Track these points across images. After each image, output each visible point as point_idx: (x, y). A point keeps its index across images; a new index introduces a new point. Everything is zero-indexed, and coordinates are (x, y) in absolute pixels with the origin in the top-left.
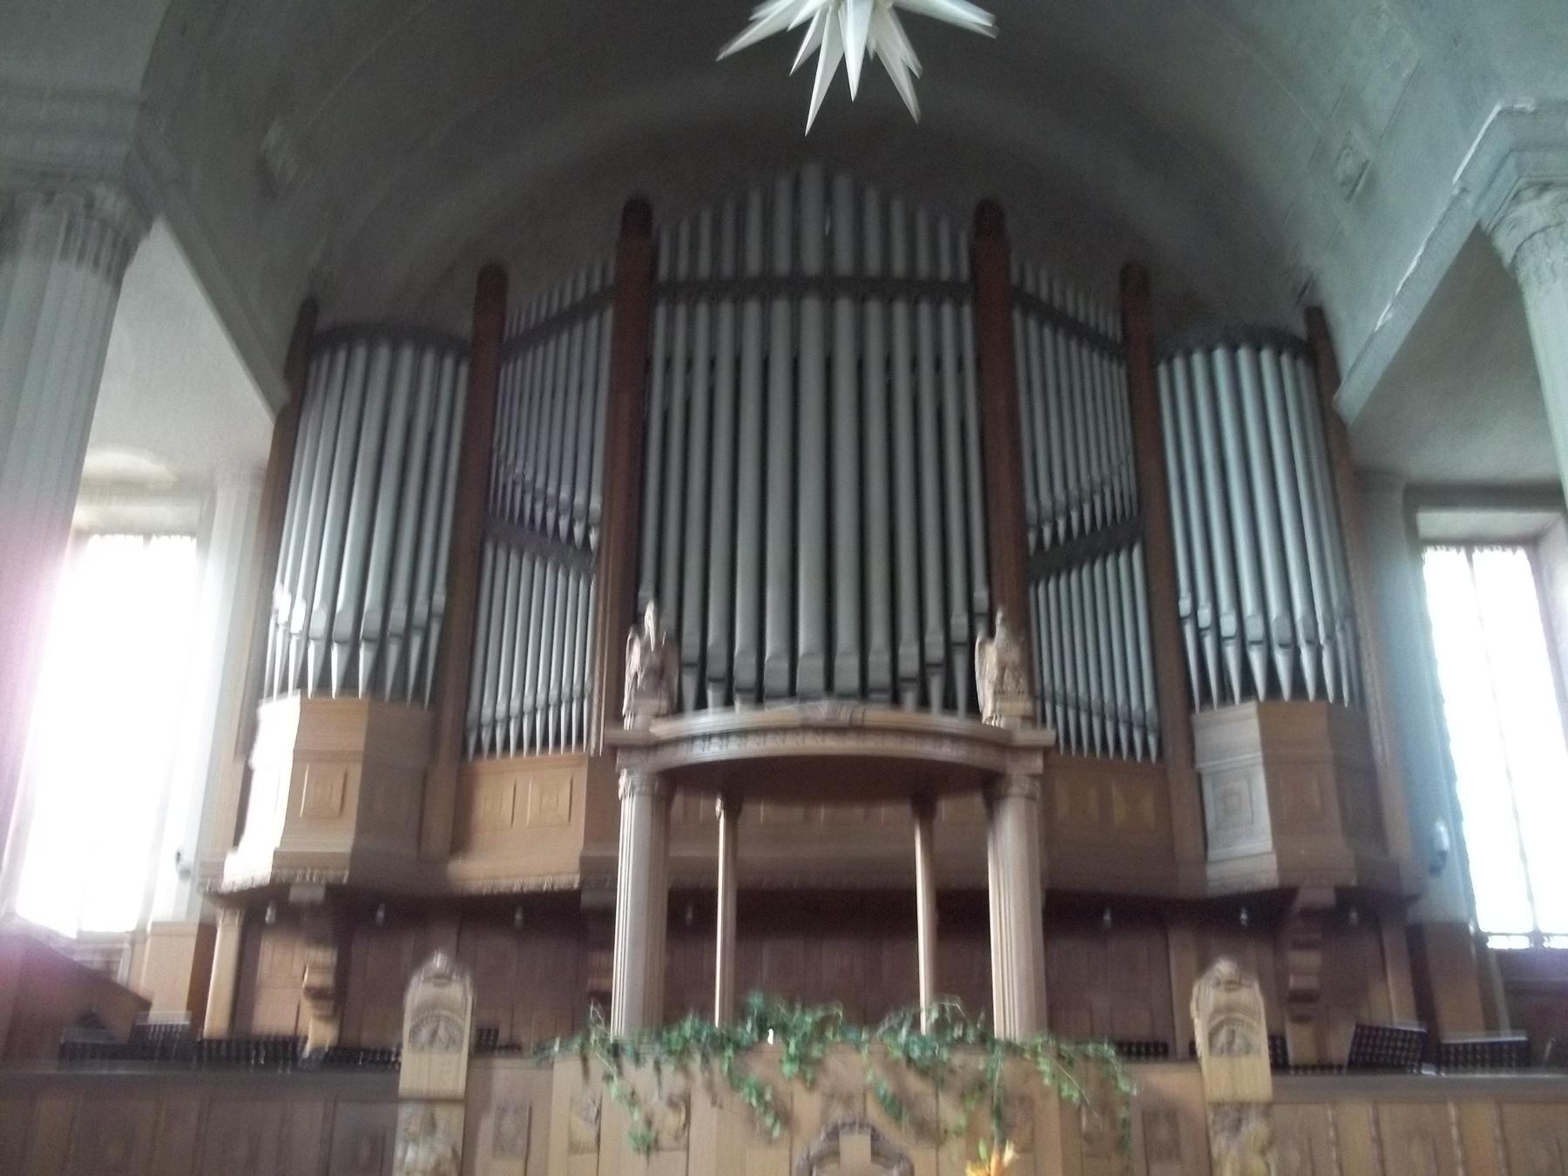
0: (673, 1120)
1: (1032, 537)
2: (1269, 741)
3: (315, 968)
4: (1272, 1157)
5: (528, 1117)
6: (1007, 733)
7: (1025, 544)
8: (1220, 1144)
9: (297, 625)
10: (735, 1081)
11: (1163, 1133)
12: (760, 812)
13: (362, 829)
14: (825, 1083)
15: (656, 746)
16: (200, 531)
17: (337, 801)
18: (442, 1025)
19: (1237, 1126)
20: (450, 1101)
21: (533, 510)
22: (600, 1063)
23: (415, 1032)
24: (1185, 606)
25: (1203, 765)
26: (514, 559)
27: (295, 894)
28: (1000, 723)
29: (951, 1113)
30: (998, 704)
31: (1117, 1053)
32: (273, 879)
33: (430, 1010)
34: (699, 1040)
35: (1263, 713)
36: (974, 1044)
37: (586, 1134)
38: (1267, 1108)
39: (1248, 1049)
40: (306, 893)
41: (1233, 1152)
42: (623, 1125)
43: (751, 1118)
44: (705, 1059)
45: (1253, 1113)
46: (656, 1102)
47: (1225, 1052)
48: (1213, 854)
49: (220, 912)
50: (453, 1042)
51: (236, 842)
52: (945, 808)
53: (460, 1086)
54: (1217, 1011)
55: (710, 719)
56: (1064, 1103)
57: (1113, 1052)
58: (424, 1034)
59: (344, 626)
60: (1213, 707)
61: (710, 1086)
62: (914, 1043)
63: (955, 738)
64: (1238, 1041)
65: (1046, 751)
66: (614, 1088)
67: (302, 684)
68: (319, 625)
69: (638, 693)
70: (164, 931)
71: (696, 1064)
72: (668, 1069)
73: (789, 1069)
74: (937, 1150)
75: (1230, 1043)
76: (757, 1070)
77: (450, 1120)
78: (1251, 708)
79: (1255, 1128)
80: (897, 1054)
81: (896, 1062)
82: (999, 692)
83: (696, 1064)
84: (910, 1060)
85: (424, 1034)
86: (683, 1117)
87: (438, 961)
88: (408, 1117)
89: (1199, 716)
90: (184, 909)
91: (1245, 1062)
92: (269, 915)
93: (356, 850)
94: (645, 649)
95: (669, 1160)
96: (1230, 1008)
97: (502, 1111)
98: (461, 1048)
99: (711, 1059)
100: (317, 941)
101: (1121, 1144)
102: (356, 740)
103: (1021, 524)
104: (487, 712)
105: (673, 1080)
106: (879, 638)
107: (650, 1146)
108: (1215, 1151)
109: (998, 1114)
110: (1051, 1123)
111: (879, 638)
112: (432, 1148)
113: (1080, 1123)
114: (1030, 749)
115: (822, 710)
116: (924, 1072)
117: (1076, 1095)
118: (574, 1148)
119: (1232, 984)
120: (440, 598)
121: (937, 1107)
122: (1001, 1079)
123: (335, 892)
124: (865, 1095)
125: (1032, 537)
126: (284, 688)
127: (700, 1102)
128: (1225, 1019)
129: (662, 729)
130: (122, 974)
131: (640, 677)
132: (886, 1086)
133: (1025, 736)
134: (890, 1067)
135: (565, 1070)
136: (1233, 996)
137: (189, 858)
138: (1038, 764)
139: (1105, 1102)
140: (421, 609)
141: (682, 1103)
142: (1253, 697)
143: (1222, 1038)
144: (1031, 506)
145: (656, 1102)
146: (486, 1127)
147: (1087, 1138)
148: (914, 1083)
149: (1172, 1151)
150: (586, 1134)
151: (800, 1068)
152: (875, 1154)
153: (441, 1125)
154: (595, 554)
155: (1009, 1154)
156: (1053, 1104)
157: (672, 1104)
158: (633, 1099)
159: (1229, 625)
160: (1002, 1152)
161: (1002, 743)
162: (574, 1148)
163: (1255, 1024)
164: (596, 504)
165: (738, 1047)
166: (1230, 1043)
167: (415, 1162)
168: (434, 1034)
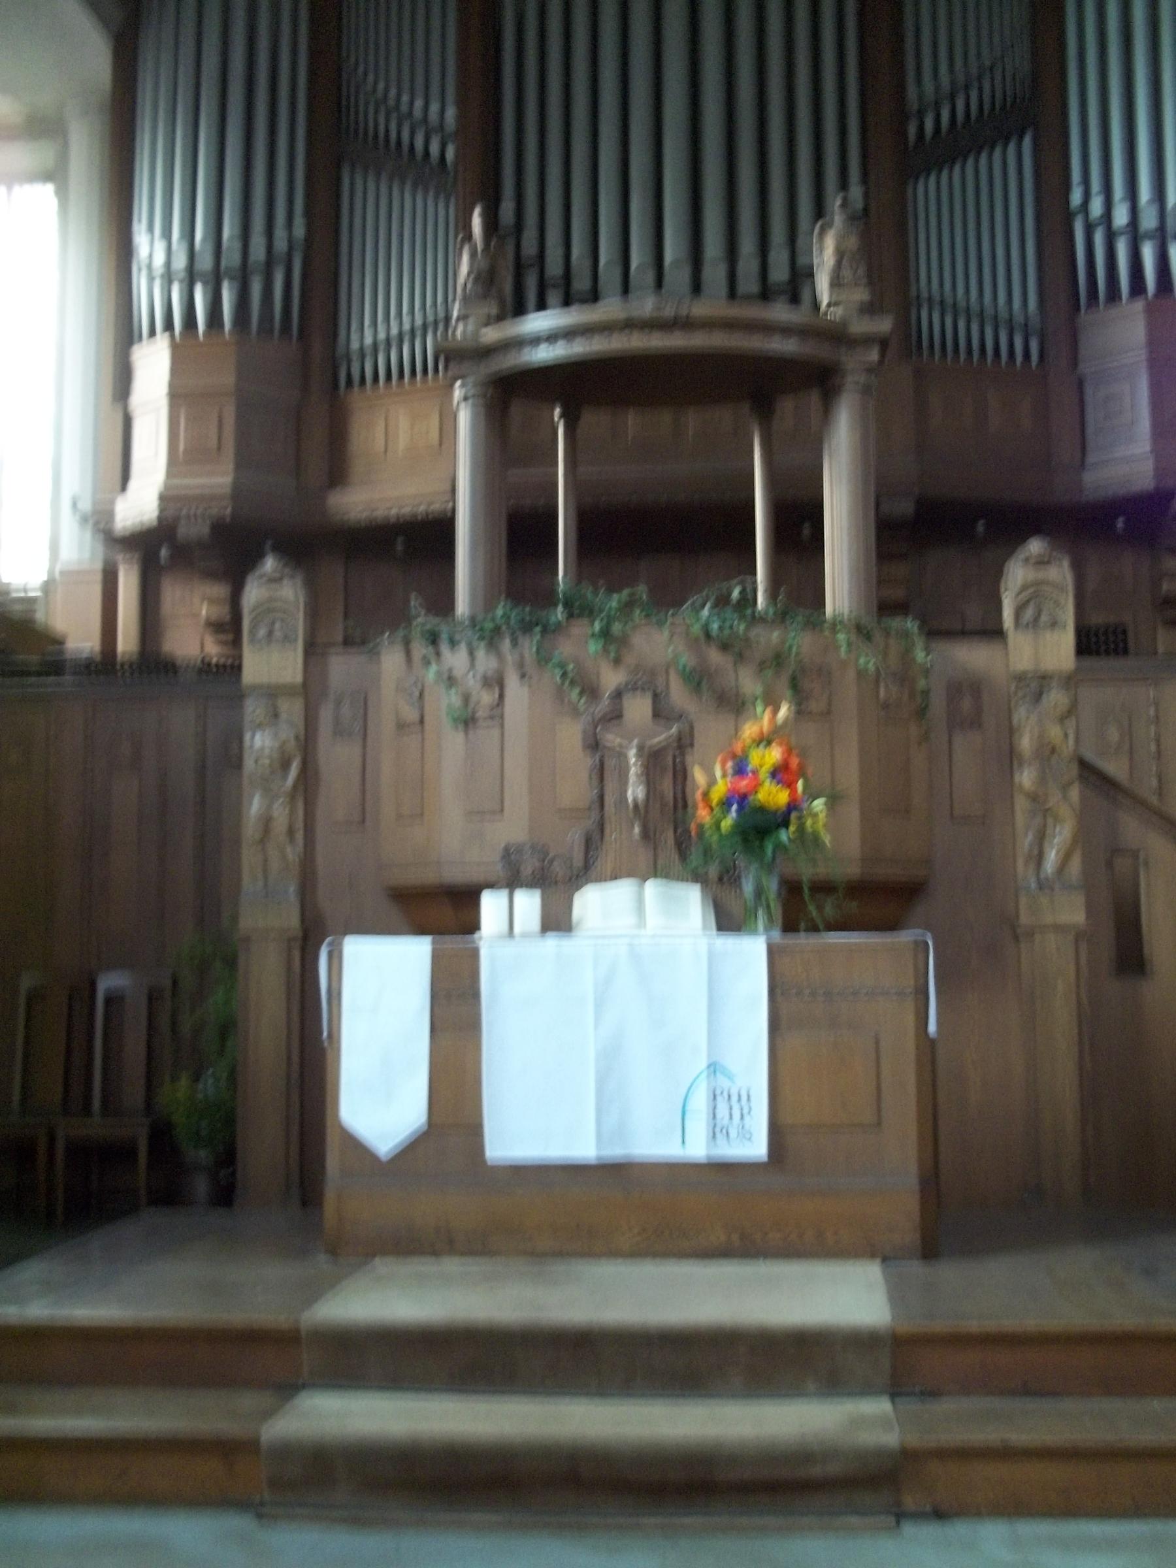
0: (487, 698)
1: (912, 130)
2: (1153, 343)
3: (212, 601)
4: (1071, 724)
5: (364, 703)
6: (844, 324)
7: (903, 134)
8: (1020, 714)
9: (159, 259)
10: (543, 659)
11: (966, 704)
12: (594, 420)
13: (241, 464)
14: (630, 659)
15: (486, 352)
16: (55, 174)
17: (213, 442)
18: (277, 625)
19: (1038, 696)
20: (286, 691)
21: (399, 133)
22: (420, 649)
23: (253, 632)
24: (1076, 197)
25: (1085, 368)
26: (371, 185)
27: (184, 531)
28: (836, 314)
29: (749, 683)
30: (833, 296)
31: (920, 628)
32: (160, 518)
33: (266, 610)
34: (508, 624)
35: (1150, 310)
36: (773, 621)
37: (411, 714)
38: (1070, 681)
39: (1054, 624)
40: (194, 530)
41: (1033, 718)
42: (444, 702)
43: (560, 695)
44: (515, 643)
45: (1054, 684)
46: (472, 683)
47: (1030, 626)
48: (1091, 459)
49: (120, 557)
50: (288, 639)
51: (124, 487)
52: (786, 406)
53: (299, 678)
54: (1024, 588)
55: (537, 322)
56: (861, 674)
57: (916, 630)
58: (262, 632)
59: (205, 263)
60: (1098, 305)
61: (521, 665)
62: (713, 621)
63: (786, 330)
64: (1044, 618)
65: (884, 343)
66: (431, 673)
67: (169, 325)
68: (180, 262)
69: (466, 299)
70: (72, 577)
71: (506, 644)
72: (481, 654)
73: (593, 647)
74: (736, 721)
75: (1036, 619)
76: (565, 648)
77: (291, 709)
78: (1139, 305)
79: (1056, 698)
80: (696, 629)
81: (697, 640)
82: (836, 282)
83: (506, 644)
84: (708, 635)
85: (262, 632)
86: (497, 696)
87: (270, 564)
88: (253, 709)
89: (1084, 316)
90: (87, 555)
91: (1049, 637)
92: (164, 553)
93: (236, 487)
94: (473, 255)
95: (487, 736)
96: (1037, 583)
97: (338, 703)
98: (296, 640)
99: (521, 640)
100: (211, 575)
101: (922, 712)
102: (228, 379)
103: (902, 115)
104: (355, 345)
105: (485, 662)
106: (748, 245)
107: (467, 721)
108: (1015, 721)
109: (795, 684)
110: (848, 691)
111: (748, 245)
112: (276, 735)
113: (878, 692)
114: (867, 341)
115: (646, 305)
116: (725, 647)
117: (871, 667)
118: (401, 726)
119: (1041, 562)
120: (299, 231)
121: (737, 680)
122: (797, 654)
123: (220, 529)
124: (667, 672)
125: (912, 130)
126: (152, 333)
127: (513, 683)
128: (1033, 596)
129: (491, 335)
130: (40, 616)
131: (469, 286)
132: (687, 659)
133: (861, 326)
134: (693, 644)
135: (391, 660)
136: (1041, 575)
137: (86, 505)
138: (874, 355)
139: (904, 675)
140: (281, 245)
141: (496, 682)
142: (1143, 296)
143: (1029, 613)
144: (912, 92)
145: (472, 683)
146: (326, 715)
147: (886, 706)
148: (715, 657)
149: (975, 722)
150: (411, 714)
151: (604, 647)
152: (656, 714)
153: (284, 716)
154: (452, 174)
155: (784, 711)
156: (851, 674)
157: (487, 682)
158: (451, 681)
159: (1121, 217)
160: (776, 710)
161: (837, 336)
162: (401, 726)
163: (1063, 602)
164: (451, 113)
165: (545, 630)
166: (1036, 619)
167: (262, 748)
168: (270, 633)
